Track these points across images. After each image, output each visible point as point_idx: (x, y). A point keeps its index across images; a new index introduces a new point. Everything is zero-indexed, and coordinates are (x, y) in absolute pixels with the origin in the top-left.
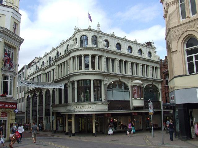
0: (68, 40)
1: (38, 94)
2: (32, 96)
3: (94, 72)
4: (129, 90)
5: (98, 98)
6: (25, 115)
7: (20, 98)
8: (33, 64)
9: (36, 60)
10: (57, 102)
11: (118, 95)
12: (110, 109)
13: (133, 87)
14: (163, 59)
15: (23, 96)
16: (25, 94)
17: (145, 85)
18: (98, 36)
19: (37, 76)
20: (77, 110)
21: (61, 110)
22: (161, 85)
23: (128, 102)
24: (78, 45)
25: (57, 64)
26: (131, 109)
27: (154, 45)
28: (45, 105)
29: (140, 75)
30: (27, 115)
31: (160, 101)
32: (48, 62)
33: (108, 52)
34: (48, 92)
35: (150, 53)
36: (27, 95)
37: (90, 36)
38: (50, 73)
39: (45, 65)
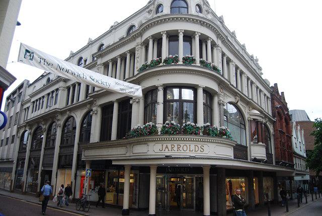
0: (107, 34)
1: (45, 127)
2: (33, 131)
6: (14, 166)
7: (8, 136)
10: (95, 136)
15: (14, 133)
16: (19, 129)
19: (49, 94)
28: (61, 147)
30: (17, 167)
36: (22, 131)
38: (28, 110)
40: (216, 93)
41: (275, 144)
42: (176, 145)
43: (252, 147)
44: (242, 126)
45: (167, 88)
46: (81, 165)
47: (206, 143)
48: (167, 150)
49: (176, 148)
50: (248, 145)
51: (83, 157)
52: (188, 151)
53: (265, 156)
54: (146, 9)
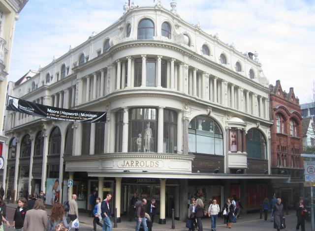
0: (106, 32)
1: (33, 136)
3: (165, 91)
4: (222, 135)
5: (171, 149)
8: (25, 80)
9: (32, 75)
10: (77, 151)
11: (205, 145)
12: (194, 170)
13: (230, 130)
14: (274, 85)
17: (247, 128)
18: (173, 23)
20: (131, 169)
21: (90, 168)
22: (271, 130)
23: (221, 158)
24: (134, 35)
25: (80, 76)
26: (225, 172)
27: (260, 59)
29: (242, 109)
31: (267, 161)
32: (58, 75)
33: (192, 55)
34: (56, 132)
35: (252, 72)
37: (159, 20)
39: (53, 81)
40: (180, 111)
41: (272, 149)
42: (135, 161)
43: (229, 156)
44: (221, 136)
45: (131, 109)
46: (66, 175)
47: (161, 159)
48: (127, 165)
49: (134, 164)
50: (225, 155)
51: (66, 169)
52: (144, 166)
53: (246, 165)
54: (117, 25)
